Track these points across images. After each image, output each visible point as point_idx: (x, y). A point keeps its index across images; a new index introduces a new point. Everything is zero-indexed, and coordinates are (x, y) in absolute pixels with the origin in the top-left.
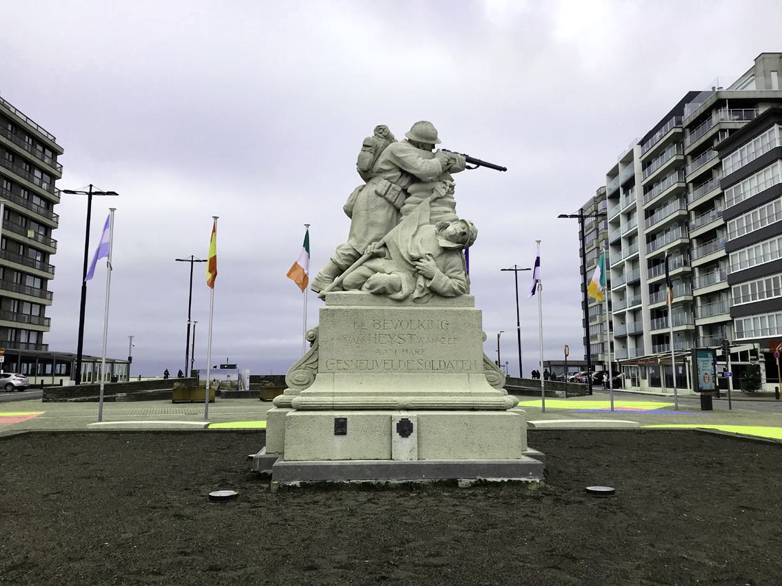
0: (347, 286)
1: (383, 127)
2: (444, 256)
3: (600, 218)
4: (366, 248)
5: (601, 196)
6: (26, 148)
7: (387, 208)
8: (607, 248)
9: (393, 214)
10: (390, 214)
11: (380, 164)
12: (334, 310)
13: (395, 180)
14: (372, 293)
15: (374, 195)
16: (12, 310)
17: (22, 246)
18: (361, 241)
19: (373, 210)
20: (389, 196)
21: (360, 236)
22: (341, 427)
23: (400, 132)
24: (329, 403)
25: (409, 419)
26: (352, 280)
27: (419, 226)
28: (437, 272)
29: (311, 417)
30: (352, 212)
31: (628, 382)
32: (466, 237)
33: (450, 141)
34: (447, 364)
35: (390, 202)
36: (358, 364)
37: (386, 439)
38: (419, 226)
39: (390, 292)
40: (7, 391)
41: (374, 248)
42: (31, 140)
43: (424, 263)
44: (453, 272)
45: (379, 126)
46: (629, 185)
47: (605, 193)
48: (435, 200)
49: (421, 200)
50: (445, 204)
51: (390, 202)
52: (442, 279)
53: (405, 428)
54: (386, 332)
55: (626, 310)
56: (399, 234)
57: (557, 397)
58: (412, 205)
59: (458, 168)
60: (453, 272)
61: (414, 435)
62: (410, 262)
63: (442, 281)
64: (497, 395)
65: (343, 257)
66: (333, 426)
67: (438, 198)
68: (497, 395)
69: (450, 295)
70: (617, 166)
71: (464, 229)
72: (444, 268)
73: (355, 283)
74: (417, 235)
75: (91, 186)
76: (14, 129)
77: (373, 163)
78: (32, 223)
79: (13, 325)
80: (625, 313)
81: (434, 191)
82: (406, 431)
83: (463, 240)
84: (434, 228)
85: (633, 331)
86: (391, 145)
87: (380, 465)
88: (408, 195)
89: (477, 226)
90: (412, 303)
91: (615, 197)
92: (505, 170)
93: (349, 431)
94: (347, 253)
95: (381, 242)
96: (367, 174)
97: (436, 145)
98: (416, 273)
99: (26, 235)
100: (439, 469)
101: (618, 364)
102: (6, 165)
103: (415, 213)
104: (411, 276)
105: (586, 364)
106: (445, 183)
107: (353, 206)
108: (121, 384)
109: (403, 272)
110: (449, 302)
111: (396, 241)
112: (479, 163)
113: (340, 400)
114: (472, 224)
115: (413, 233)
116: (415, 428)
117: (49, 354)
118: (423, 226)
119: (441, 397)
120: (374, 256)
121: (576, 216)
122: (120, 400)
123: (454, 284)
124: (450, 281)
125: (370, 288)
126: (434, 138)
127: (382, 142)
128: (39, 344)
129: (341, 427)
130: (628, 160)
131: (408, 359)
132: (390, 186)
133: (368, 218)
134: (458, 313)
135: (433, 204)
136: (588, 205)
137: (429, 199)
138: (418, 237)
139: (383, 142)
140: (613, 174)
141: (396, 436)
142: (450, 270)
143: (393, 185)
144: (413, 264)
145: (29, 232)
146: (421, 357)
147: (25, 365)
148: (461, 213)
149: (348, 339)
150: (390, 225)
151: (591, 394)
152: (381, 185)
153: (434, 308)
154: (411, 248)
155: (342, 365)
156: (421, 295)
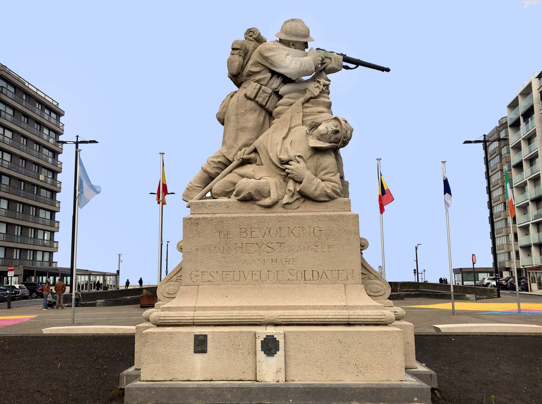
0: (217, 194)
1: (253, 30)
2: (316, 157)
3: (502, 143)
4: (236, 154)
5: (503, 125)
6: (37, 112)
7: (258, 112)
8: (510, 170)
9: (265, 118)
10: (262, 118)
11: (250, 68)
12: (199, 219)
13: (264, 82)
14: (238, 200)
15: (244, 99)
16: (30, 236)
17: (23, 183)
18: (231, 147)
19: (243, 114)
20: (259, 99)
21: (229, 142)
22: (201, 345)
23: (271, 35)
24: (189, 318)
25: (275, 336)
26: (221, 188)
27: (290, 129)
28: (308, 174)
29: (171, 333)
30: (224, 119)
31: (534, 286)
32: (338, 136)
33: (325, 39)
34: (320, 275)
35: (262, 107)
36: (224, 276)
37: (250, 358)
38: (290, 129)
39: (257, 198)
40: (32, 298)
41: (244, 154)
42: (40, 106)
43: (293, 166)
44: (325, 174)
45: (249, 30)
46: (529, 113)
47: (506, 123)
48: (307, 101)
49: (294, 101)
50: (318, 104)
51: (262, 107)
52: (313, 182)
53: (270, 346)
54: (253, 240)
55: (521, 139)
56: (269, 137)
57: (467, 300)
58: (285, 107)
59: (334, 68)
60: (325, 174)
61: (280, 353)
62: (280, 166)
63: (317, 183)
64: (376, 307)
65: (213, 165)
66: (192, 343)
67: (311, 98)
68: (376, 307)
69: (322, 199)
70: (517, 98)
71: (337, 127)
72: (316, 170)
73: (224, 191)
74: (286, 138)
75: (77, 136)
76: (28, 98)
77: (243, 67)
78: (43, 169)
79: (31, 247)
80: (528, 225)
81: (307, 91)
82: (271, 349)
83: (337, 139)
84: (305, 129)
85: (537, 241)
86: (260, 46)
87: (242, 388)
88: (280, 97)
89: (352, 123)
90: (281, 209)
91: (516, 125)
92: (388, 70)
93: (209, 349)
94: (217, 160)
95: (252, 147)
96: (237, 78)
97: (309, 43)
98: (287, 177)
99: (39, 179)
100: (308, 393)
101: (524, 270)
102: (22, 125)
103: (286, 116)
104: (282, 180)
105: (494, 270)
106: (319, 82)
107: (224, 114)
108: (110, 292)
109: (275, 177)
110: (322, 206)
111: (266, 145)
112: (358, 63)
113: (201, 315)
114: (346, 122)
115: (283, 136)
116: (281, 346)
117: (57, 269)
118: (295, 128)
119: (312, 311)
120: (245, 162)
121: (480, 142)
122: (100, 306)
123: (328, 187)
124: (323, 184)
125: (236, 195)
126: (307, 35)
127: (251, 45)
128: (51, 262)
129: (201, 345)
130: (527, 91)
131: (277, 269)
132: (260, 88)
133: (238, 123)
134: (332, 219)
135: (306, 105)
136: (492, 134)
137: (302, 99)
138: (288, 140)
139: (253, 45)
140: (514, 105)
141: (261, 355)
142: (323, 173)
143: (263, 87)
144: (282, 167)
145: (41, 176)
146: (292, 267)
147: (41, 277)
148: (336, 111)
149: (213, 249)
150: (260, 129)
151: (499, 296)
152: (251, 88)
153: (305, 214)
154: (281, 150)
155: (207, 277)
156: (291, 201)
